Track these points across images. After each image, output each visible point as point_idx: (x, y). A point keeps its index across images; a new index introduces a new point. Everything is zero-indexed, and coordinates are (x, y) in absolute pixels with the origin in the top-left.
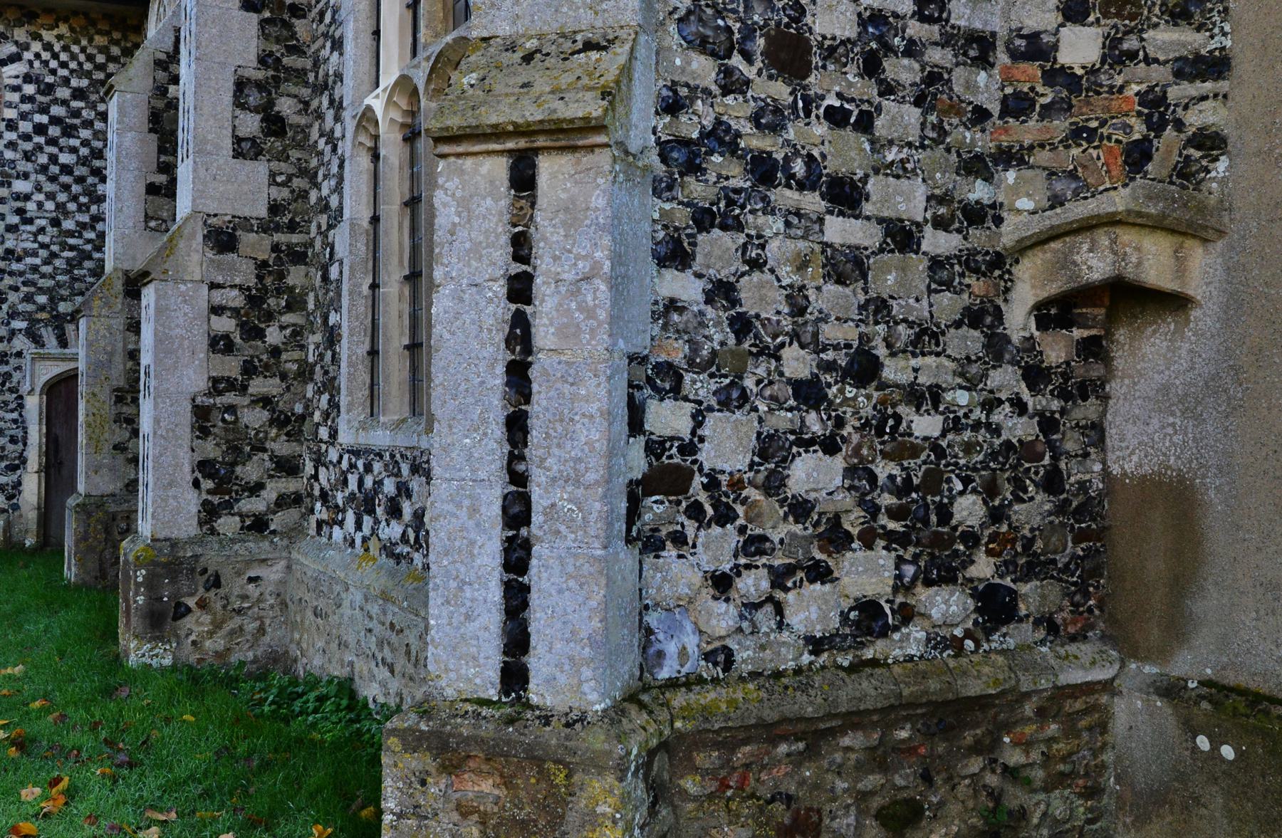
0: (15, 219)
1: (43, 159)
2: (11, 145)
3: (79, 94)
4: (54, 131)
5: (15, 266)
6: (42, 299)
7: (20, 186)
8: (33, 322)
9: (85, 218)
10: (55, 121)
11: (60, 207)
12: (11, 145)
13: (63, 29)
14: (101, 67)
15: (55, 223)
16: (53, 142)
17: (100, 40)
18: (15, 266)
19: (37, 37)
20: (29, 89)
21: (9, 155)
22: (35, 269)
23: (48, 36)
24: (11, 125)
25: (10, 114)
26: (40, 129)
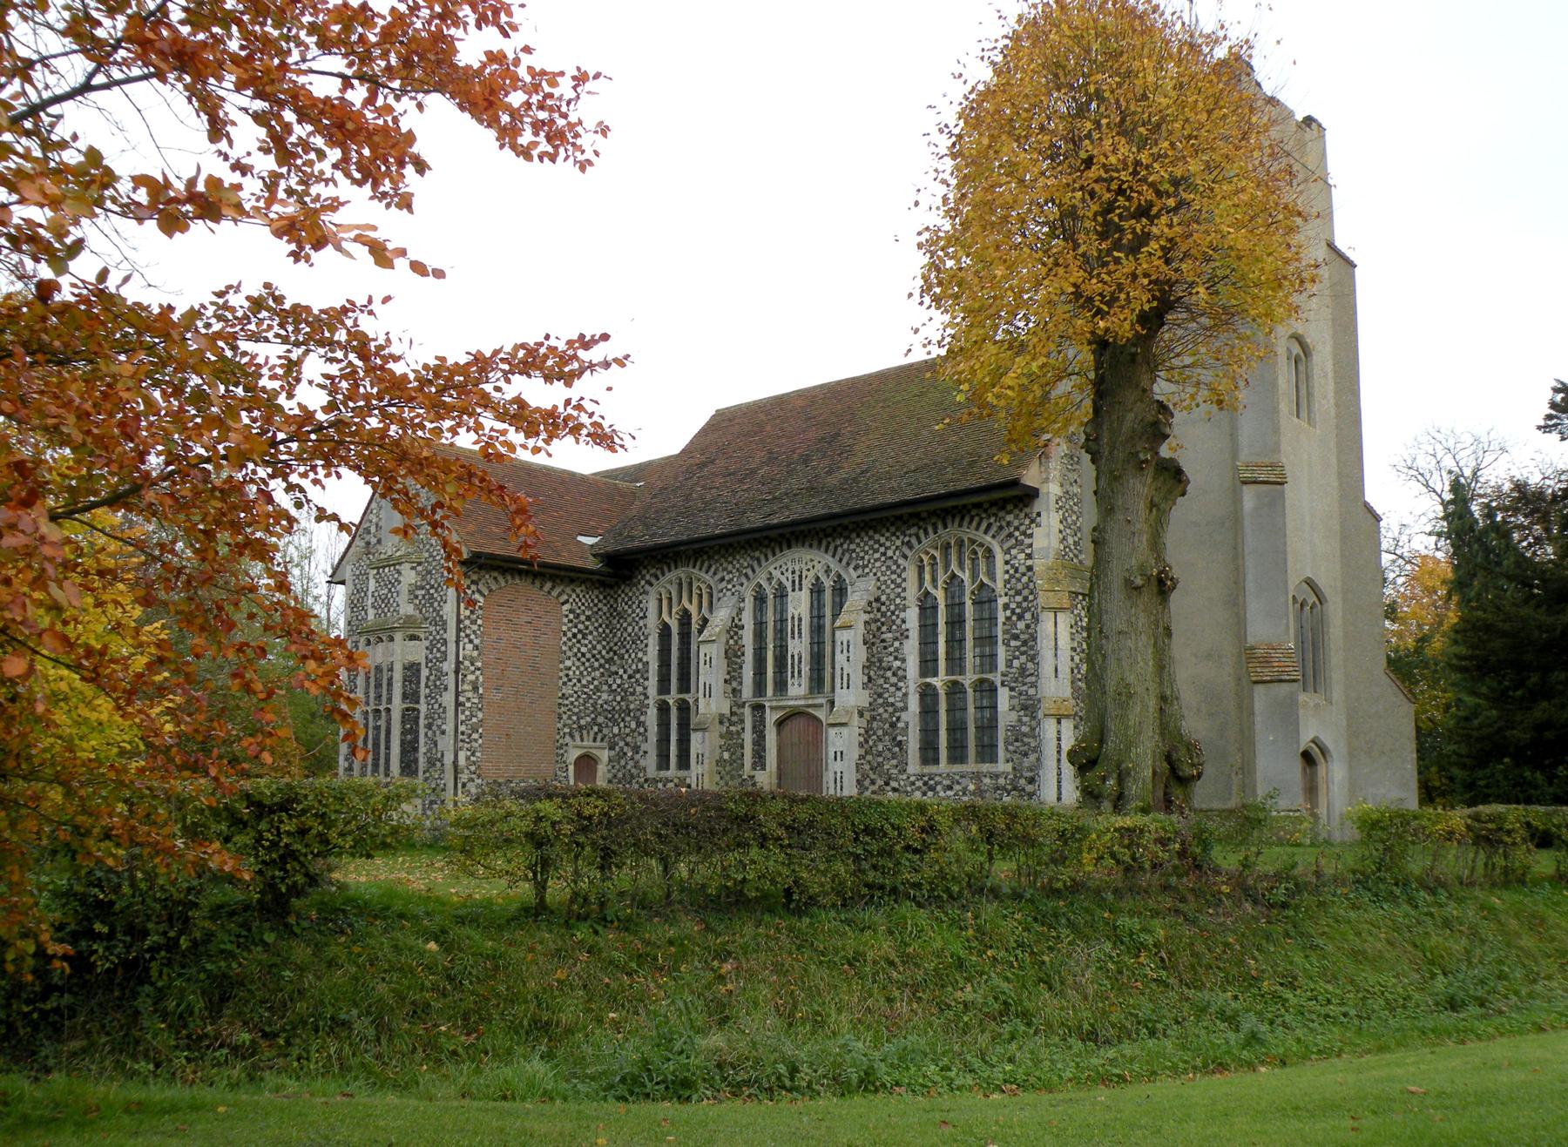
0: (565, 679)
1: (575, 650)
2: (565, 643)
3: (588, 619)
4: (580, 636)
5: (566, 702)
6: (575, 718)
7: (568, 663)
8: (571, 729)
9: (589, 679)
10: (580, 631)
11: (581, 673)
12: (565, 643)
13: (583, 588)
14: (596, 605)
15: (579, 681)
16: (579, 642)
17: (596, 592)
18: (566, 702)
19: (574, 591)
20: (571, 616)
21: (564, 648)
22: (572, 703)
23: (578, 591)
24: (565, 635)
25: (564, 628)
26: (574, 636)
